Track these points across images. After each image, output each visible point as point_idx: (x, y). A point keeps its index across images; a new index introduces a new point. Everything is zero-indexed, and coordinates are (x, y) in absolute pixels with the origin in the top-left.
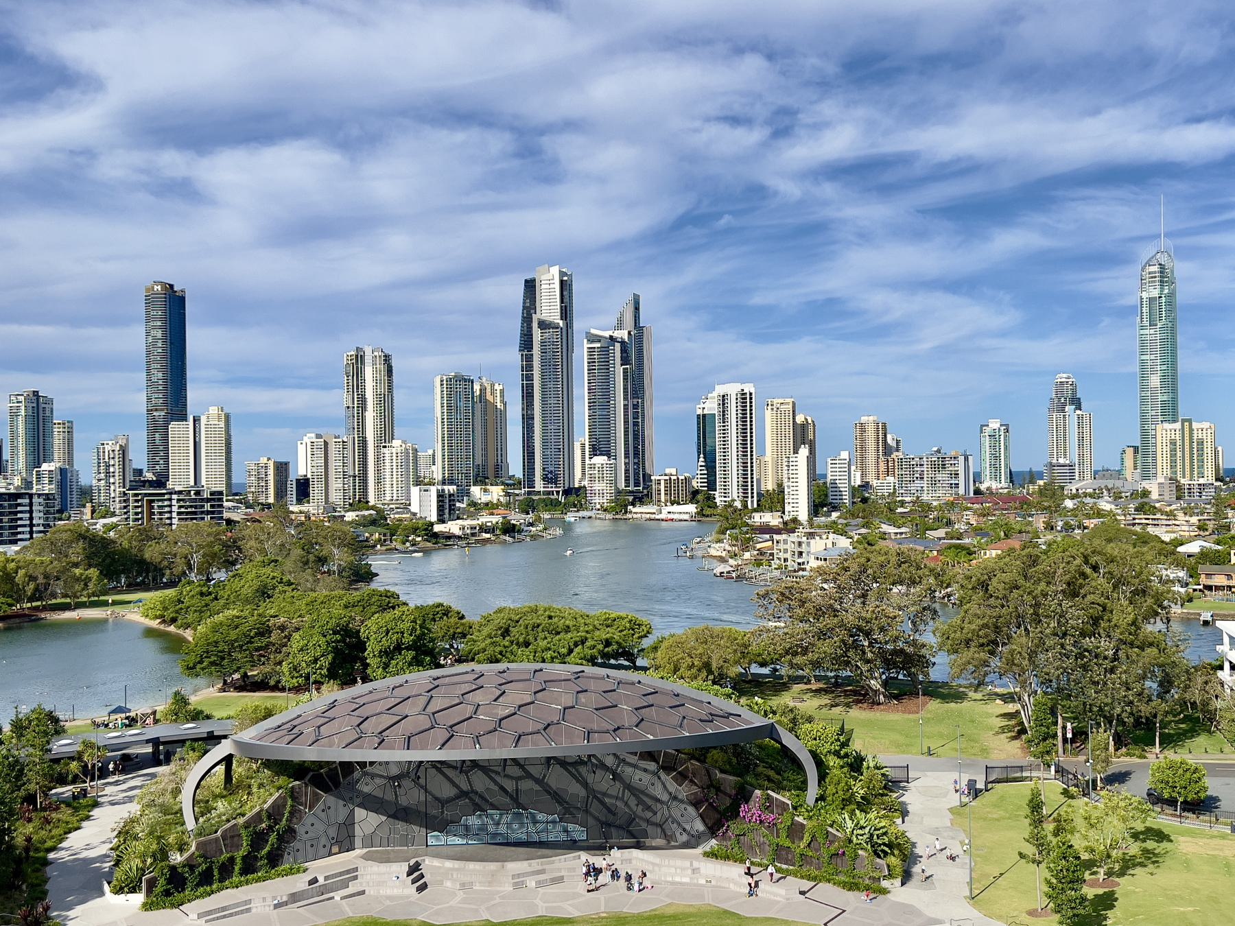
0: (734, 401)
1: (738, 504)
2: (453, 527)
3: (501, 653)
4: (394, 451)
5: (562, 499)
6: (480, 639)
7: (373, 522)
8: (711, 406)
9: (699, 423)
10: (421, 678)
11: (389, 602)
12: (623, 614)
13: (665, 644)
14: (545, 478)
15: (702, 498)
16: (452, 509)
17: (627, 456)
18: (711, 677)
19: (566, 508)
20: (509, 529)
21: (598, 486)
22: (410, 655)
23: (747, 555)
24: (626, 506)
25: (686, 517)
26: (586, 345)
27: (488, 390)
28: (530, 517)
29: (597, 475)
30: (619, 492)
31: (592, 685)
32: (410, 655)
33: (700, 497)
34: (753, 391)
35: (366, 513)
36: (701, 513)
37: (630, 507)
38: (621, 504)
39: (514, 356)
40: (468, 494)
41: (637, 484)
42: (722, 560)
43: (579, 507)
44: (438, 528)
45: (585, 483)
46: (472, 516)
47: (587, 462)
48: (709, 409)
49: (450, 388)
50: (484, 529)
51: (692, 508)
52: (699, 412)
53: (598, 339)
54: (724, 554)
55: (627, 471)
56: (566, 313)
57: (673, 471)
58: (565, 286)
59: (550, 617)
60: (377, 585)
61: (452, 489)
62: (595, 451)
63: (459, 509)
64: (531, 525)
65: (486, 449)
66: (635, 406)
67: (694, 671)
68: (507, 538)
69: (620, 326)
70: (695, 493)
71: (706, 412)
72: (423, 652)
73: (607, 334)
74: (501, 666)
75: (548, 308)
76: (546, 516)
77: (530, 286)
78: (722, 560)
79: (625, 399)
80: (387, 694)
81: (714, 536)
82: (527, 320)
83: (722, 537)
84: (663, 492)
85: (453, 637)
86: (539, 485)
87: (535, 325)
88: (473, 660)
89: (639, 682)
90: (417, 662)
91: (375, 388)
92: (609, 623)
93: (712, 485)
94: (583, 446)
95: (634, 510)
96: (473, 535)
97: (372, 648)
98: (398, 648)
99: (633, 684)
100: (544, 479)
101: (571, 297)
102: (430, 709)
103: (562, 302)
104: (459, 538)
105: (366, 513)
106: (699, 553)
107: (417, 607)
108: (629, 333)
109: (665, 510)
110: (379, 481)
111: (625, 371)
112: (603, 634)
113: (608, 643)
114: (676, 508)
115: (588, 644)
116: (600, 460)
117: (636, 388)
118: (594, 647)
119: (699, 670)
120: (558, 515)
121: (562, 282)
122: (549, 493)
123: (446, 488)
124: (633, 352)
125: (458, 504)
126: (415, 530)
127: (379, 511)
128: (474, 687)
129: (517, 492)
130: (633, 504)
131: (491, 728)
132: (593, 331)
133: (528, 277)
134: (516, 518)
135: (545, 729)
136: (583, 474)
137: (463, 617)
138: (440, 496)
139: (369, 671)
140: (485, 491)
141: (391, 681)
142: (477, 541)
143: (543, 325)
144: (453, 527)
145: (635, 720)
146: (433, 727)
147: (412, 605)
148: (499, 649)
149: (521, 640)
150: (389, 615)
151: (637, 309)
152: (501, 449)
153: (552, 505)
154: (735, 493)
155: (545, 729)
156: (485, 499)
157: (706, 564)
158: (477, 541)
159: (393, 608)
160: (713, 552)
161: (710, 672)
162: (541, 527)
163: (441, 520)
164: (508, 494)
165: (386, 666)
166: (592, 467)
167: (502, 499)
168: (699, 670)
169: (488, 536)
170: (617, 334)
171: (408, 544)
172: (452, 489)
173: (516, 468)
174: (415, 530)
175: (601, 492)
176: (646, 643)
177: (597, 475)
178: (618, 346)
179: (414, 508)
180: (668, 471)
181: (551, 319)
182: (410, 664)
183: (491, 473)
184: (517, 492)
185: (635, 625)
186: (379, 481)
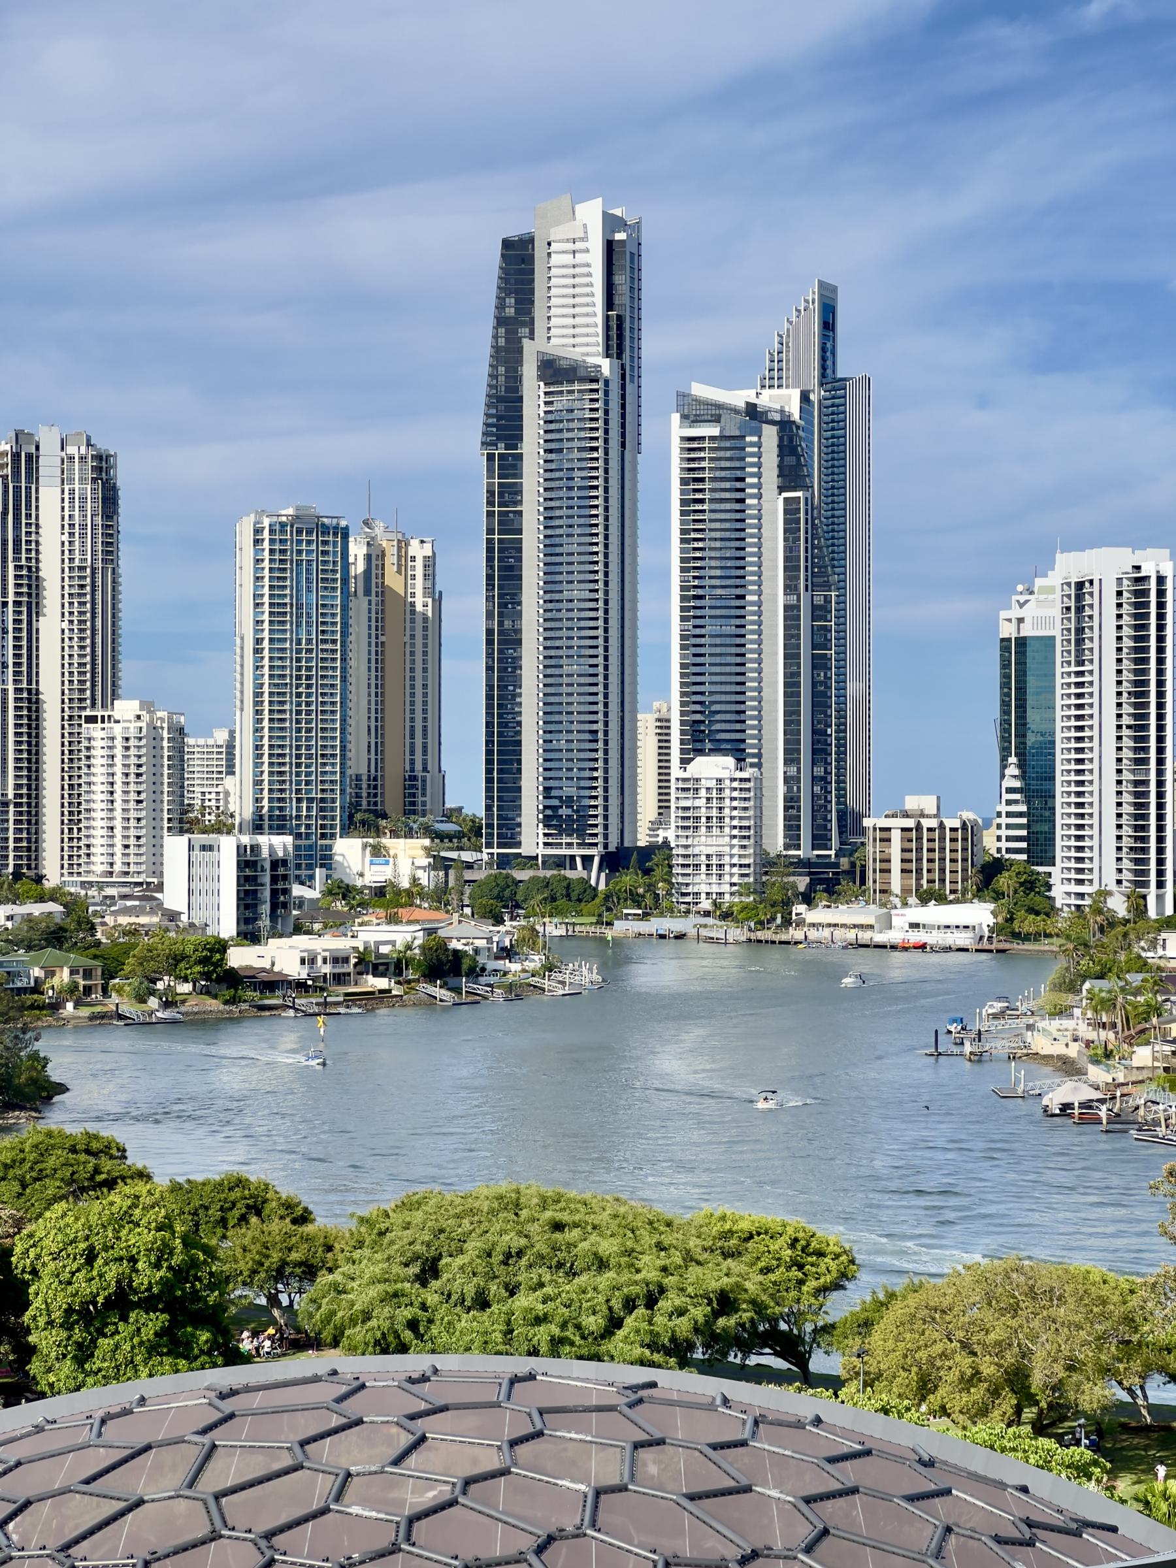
0: (1110, 600)
1: (1118, 906)
2: (283, 955)
3: (413, 1325)
4: (117, 730)
5: (598, 879)
6: (360, 1282)
7: (55, 937)
8: (1040, 615)
9: (1005, 665)
10: (181, 1393)
11: (95, 1169)
12: (772, 1218)
13: (897, 1311)
14: (551, 819)
15: (1011, 883)
16: (280, 902)
17: (791, 757)
18: (1029, 1413)
19: (611, 904)
20: (444, 965)
21: (705, 844)
22: (152, 1323)
23: (1143, 1056)
24: (787, 904)
25: (963, 939)
26: (677, 430)
27: (391, 560)
28: (507, 931)
29: (707, 812)
30: (767, 864)
31: (679, 1426)
32: (152, 1323)
33: (1004, 881)
34: (1167, 570)
35: (36, 909)
36: (1007, 929)
37: (800, 908)
38: (772, 897)
40: (326, 861)
41: (820, 840)
42: (1068, 1068)
43: (651, 906)
44: (240, 957)
45: (669, 834)
46: (338, 924)
47: (676, 771)
48: (1039, 621)
49: (280, 555)
50: (370, 963)
51: (981, 914)
52: (1008, 631)
53: (714, 412)
54: (1073, 1051)
55: (791, 802)
56: (620, 336)
57: (928, 803)
58: (618, 258)
59: (558, 1227)
60: (64, 1119)
61: (279, 844)
62: (700, 739)
63: (300, 903)
64: (507, 953)
65: (378, 730)
66: (820, 612)
67: (978, 1393)
69: (774, 380)
70: (992, 869)
71: (1027, 631)
72: (190, 1316)
73: (738, 398)
74: (415, 1362)
75: (570, 322)
76: (553, 928)
77: (519, 261)
78: (1068, 1068)
79: (790, 588)
80: (85, 1435)
81: (1045, 995)
82: (507, 356)
83: (1070, 999)
84: (896, 866)
85: (279, 1274)
86: (533, 839)
87: (529, 371)
88: (335, 1343)
89: (818, 1421)
90: (173, 1347)
91: (66, 550)
92: (732, 1244)
93: (1040, 846)
94: (663, 725)
95: (812, 916)
96: (339, 979)
97: (46, 1298)
98: (121, 1302)
99: (799, 1425)
100: (547, 821)
102: (211, 1482)
103: (609, 304)
104: (301, 986)
105: (36, 909)
106: (999, 1046)
107: (176, 1188)
108: (805, 397)
109: (903, 917)
110: (74, 816)
111: (791, 509)
112: (714, 1277)
113: (725, 1302)
114: (934, 913)
115: (664, 1305)
116: (713, 768)
117: (821, 554)
118: (681, 1312)
119: (995, 1393)
120: (585, 925)
121: (610, 247)
122: (561, 863)
123: (263, 840)
124: (817, 452)
125: (297, 890)
126: (175, 962)
127: (73, 905)
128: (335, 1421)
129: (467, 856)
130: (808, 899)
131: (384, 1543)
132: (700, 390)
133: (514, 231)
134: (466, 934)
135: (540, 1550)
136: (663, 806)
137: (304, 1218)
138: (248, 863)
139: (35, 1367)
141: (99, 1398)
142: (351, 999)
143: (555, 372)
144: (283, 955)
145: (804, 1532)
146: (214, 1536)
147: (161, 1181)
148: (407, 1313)
149: (470, 1291)
150: (95, 1208)
151: (828, 326)
152: (424, 731)
153: (567, 897)
154: (1108, 869)
155: (540, 1550)
157: (1019, 1077)
158: (351, 999)
159: (110, 1184)
160: (1041, 1044)
161: (1026, 1397)
162: (536, 961)
163: (249, 935)
164: (441, 864)
165: (83, 1354)
166: (691, 787)
167: (424, 878)
168: (995, 1393)
169: (382, 983)
170: (768, 399)
171: (153, 1002)
172: (279, 844)
173: (465, 788)
174: (175, 962)
175: (715, 864)
176: (840, 1307)
177: (707, 812)
178: (770, 435)
179: (174, 897)
180: (912, 803)
181: (576, 354)
182: (152, 1350)
183: (392, 799)
184: (467, 856)
185: (806, 1251)
186: (74, 816)
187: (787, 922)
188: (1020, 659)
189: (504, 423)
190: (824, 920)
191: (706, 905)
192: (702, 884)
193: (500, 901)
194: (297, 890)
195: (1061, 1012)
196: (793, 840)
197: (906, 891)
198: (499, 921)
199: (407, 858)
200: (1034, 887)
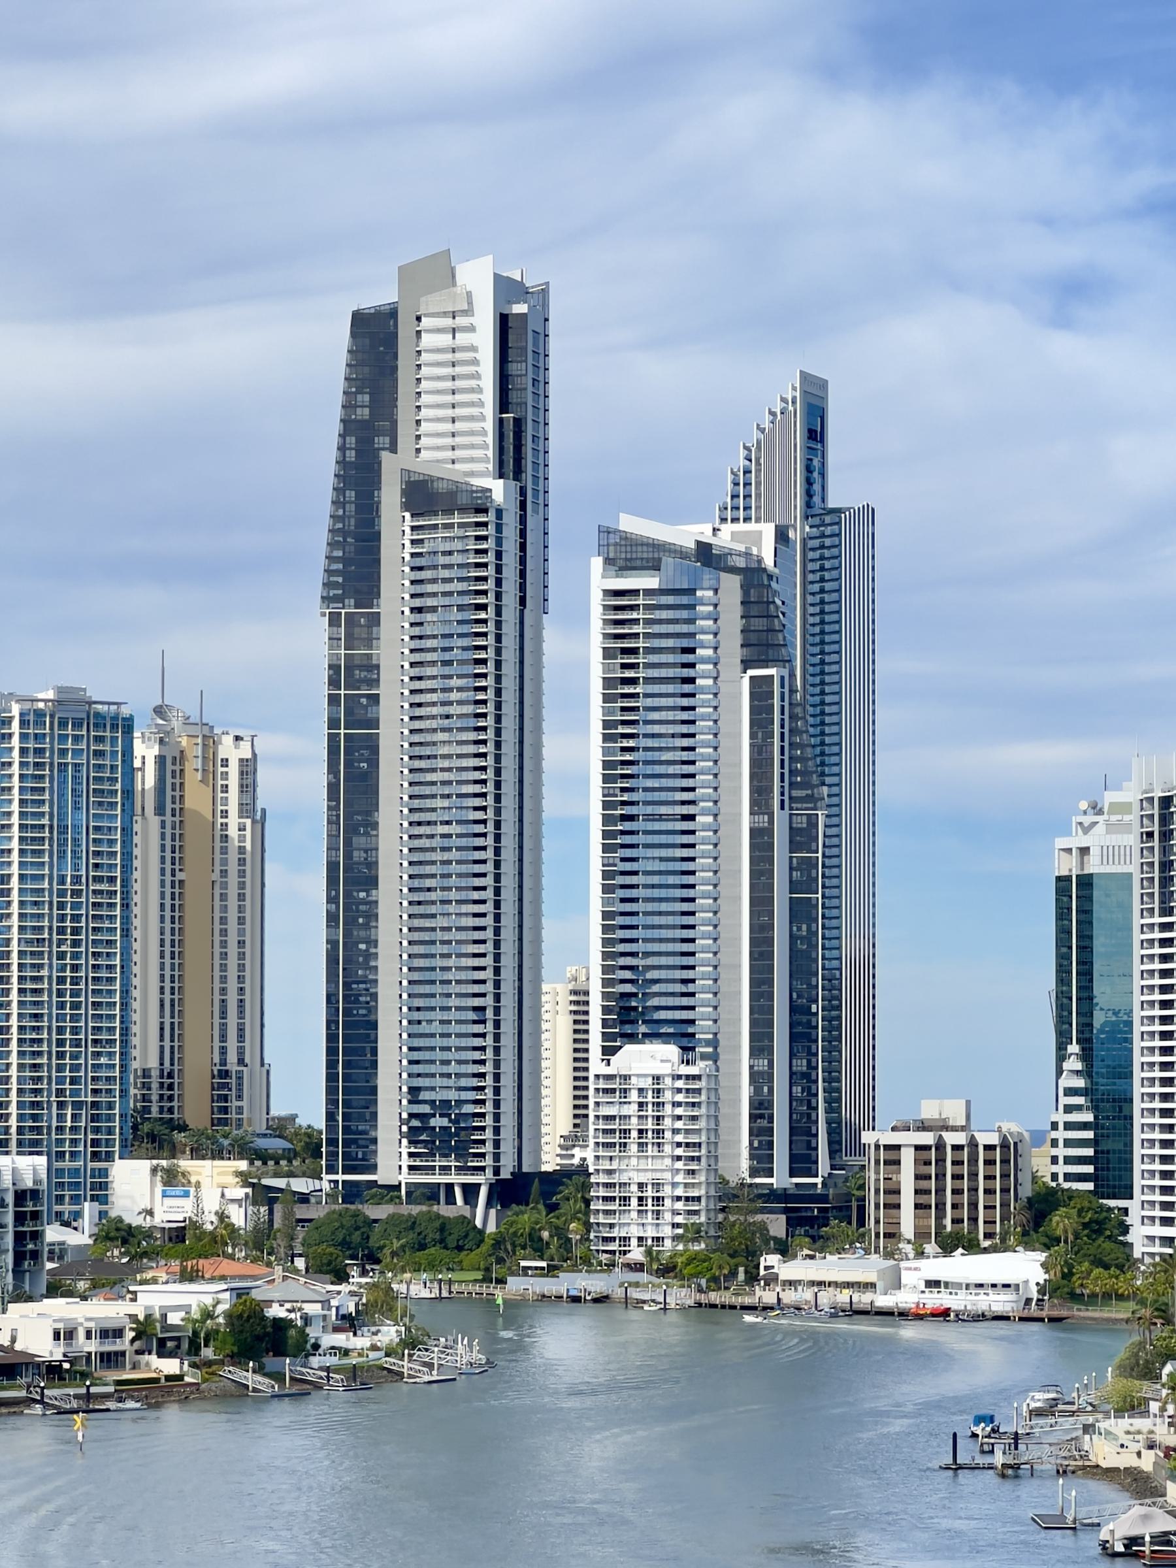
9: (1062, 913)
17: (761, 1044)
19: (500, 1257)
20: (260, 1339)
21: (635, 1169)
24: (752, 1256)
25: (1000, 1302)
26: (600, 579)
27: (193, 764)
28: (345, 1296)
30: (728, 1196)
33: (1061, 1221)
37: (771, 1260)
39: (305, 641)
40: (100, 1191)
41: (802, 1162)
42: (1141, 1486)
45: (584, 1154)
46: (109, 1281)
47: (596, 1066)
50: (152, 1335)
51: (1026, 1267)
52: (1068, 866)
54: (1147, 1462)
55: (761, 1110)
56: (517, 447)
57: (954, 1112)
62: (628, 1019)
64: (350, 1323)
66: (801, 838)
68: (250, 1378)
69: (740, 506)
71: (1094, 866)
75: (449, 429)
76: (416, 1287)
78: (1141, 1486)
82: (358, 475)
83: (1145, 1388)
84: (907, 1199)
86: (393, 1162)
87: (390, 496)
93: (1112, 1172)
94: (580, 998)
95: (788, 1270)
96: (111, 1360)
100: (413, 1135)
101: (540, 383)
103: (503, 403)
104: (53, 1371)
108: (782, 536)
114: (961, 1266)
116: (649, 1060)
117: (808, 753)
120: (466, 1282)
121: (504, 323)
122: (431, 1194)
129: (300, 1185)
130: (784, 1250)
132: (629, 524)
134: (289, 1294)
140: (171, 1178)
143: (424, 497)
151: (816, 436)
152: (241, 1009)
153: (439, 1241)
156: (170, 1211)
160: (1104, 1453)
162: (389, 1334)
166: (616, 1086)
167: (237, 1216)
169: (170, 1366)
170: (727, 537)
173: (298, 1092)
175: (652, 1193)
178: (731, 585)
180: (929, 1110)
187: (753, 1278)
188: (1077, 898)
189: (354, 571)
190: (806, 1275)
191: (637, 1254)
192: (633, 1226)
193: (345, 1247)
194: (53, 1233)
195: (1133, 1407)
196: (762, 1160)
197: (921, 1235)
198: (341, 1277)
199: (215, 1188)
200: (1103, 1232)
